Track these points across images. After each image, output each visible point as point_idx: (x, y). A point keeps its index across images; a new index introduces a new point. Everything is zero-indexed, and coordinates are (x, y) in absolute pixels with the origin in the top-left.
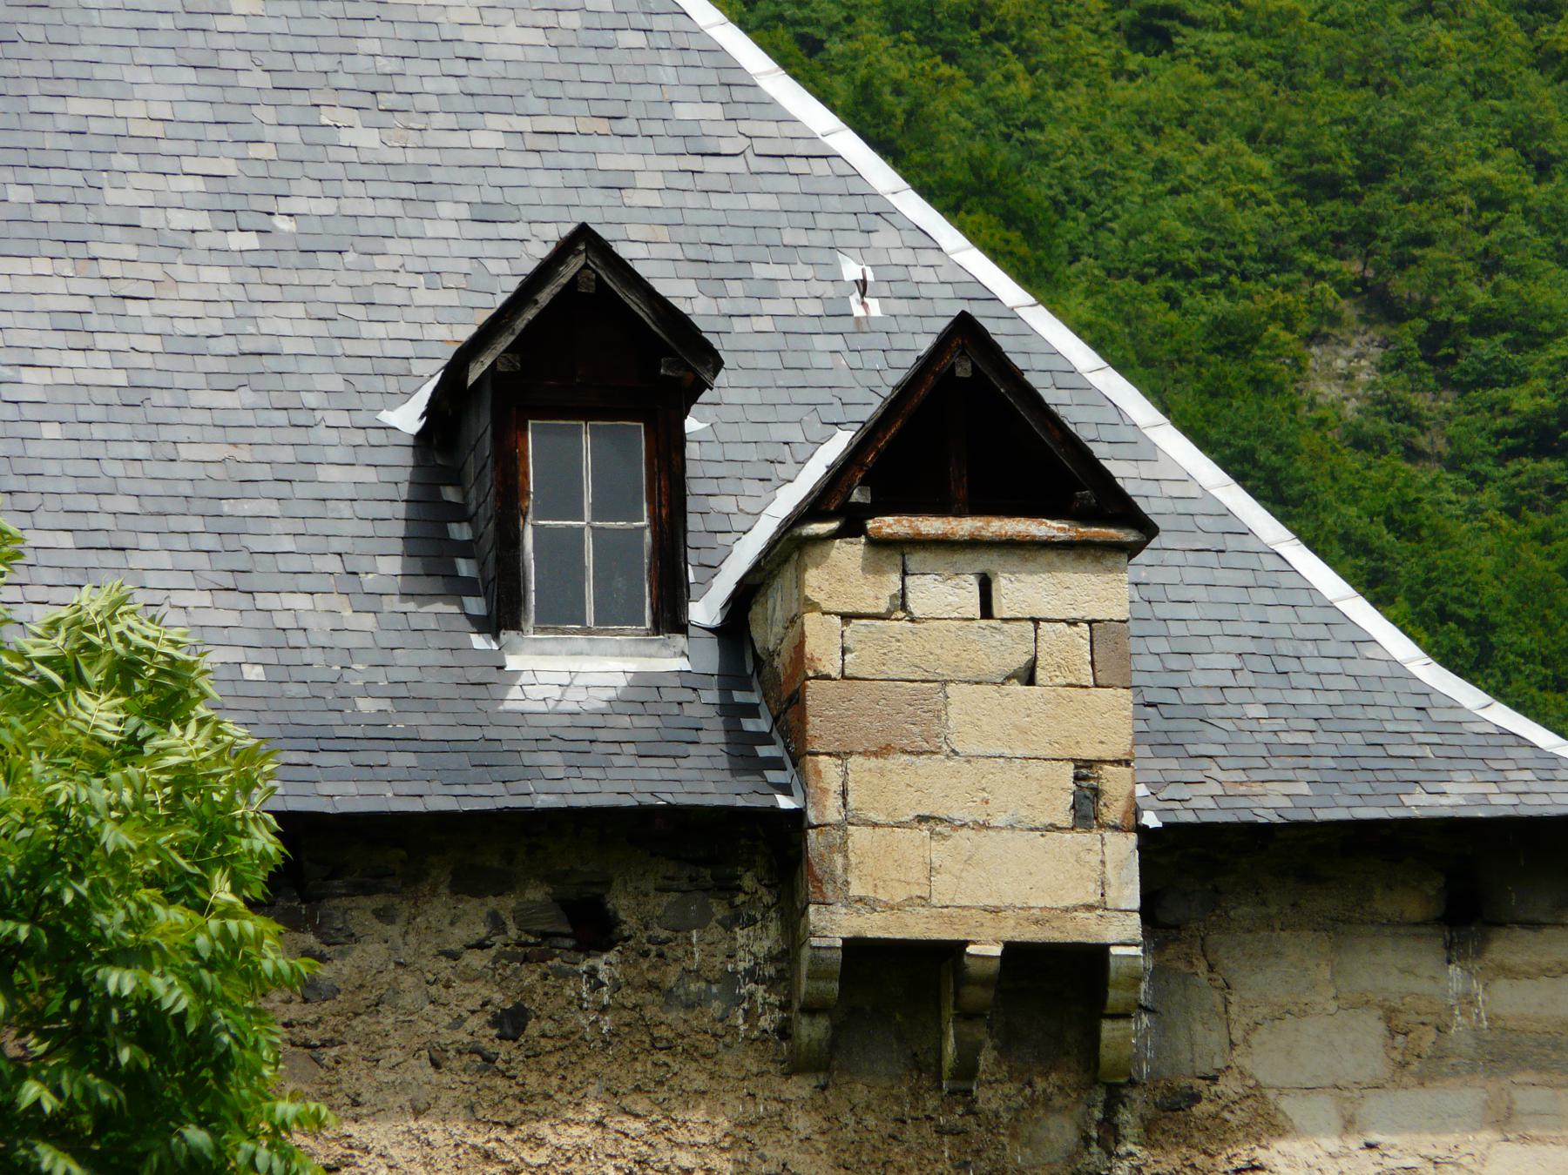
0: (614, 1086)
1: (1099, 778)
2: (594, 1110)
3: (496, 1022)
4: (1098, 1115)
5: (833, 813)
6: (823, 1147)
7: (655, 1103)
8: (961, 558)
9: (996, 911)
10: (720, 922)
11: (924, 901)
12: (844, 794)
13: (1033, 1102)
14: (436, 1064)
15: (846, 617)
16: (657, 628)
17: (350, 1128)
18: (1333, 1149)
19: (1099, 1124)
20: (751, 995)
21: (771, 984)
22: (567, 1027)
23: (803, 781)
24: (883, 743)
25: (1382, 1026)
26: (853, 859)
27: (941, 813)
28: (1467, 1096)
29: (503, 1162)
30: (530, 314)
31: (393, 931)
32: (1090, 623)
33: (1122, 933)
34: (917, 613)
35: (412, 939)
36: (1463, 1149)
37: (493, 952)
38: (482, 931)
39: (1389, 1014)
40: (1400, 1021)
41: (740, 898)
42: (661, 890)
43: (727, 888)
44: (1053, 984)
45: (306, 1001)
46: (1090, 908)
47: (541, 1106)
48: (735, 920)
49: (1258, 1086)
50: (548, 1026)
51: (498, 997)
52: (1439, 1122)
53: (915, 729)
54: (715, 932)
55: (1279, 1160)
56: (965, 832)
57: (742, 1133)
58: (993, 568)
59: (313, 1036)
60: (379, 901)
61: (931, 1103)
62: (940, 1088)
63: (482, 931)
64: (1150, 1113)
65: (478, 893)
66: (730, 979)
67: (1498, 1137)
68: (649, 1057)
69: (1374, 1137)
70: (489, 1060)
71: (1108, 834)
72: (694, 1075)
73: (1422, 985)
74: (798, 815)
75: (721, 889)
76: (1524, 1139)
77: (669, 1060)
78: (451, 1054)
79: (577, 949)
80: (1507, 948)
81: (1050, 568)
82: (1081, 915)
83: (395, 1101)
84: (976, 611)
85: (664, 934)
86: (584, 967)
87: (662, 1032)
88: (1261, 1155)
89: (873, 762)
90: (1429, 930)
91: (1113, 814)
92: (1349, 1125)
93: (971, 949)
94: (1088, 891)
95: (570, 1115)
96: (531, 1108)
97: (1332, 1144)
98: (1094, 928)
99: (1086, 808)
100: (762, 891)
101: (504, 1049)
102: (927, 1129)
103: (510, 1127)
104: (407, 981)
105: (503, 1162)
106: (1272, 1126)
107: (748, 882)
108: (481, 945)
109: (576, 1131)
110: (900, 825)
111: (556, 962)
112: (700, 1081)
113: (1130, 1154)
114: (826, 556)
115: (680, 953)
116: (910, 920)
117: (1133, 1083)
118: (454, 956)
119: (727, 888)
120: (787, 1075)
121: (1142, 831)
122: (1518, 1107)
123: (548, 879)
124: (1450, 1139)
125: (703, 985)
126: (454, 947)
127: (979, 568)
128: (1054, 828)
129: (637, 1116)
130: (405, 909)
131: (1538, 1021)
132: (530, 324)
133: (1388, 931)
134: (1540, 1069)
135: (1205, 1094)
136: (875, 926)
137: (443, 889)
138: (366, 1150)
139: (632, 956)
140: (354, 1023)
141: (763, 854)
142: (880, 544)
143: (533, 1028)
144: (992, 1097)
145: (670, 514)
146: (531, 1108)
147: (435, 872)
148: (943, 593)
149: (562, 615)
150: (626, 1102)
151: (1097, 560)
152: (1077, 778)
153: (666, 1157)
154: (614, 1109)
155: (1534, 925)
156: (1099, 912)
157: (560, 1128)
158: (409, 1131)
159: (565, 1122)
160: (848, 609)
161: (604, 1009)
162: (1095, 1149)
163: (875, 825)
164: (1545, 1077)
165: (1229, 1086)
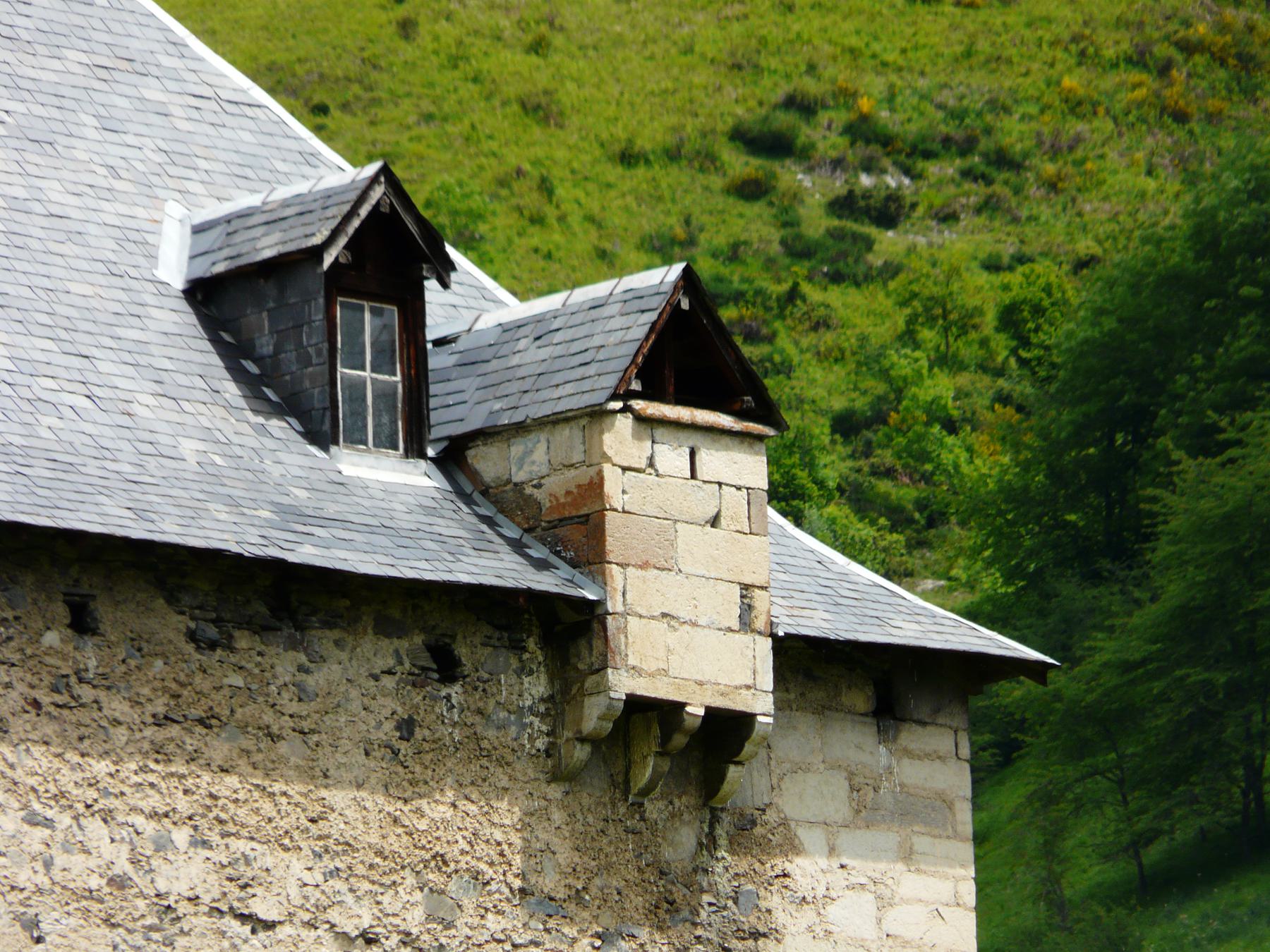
0: (461, 779)
1: (751, 598)
2: (450, 794)
3: (398, 728)
4: (706, 830)
5: (620, 608)
6: (567, 835)
7: (482, 794)
8: (683, 435)
9: (701, 684)
10: (515, 671)
11: (665, 672)
12: (624, 594)
13: (673, 816)
14: (367, 754)
15: (625, 469)
16: (407, 454)
17: (324, 793)
18: (824, 867)
19: (707, 835)
20: (531, 723)
21: (543, 717)
22: (437, 736)
23: (600, 579)
24: (644, 558)
25: (846, 784)
26: (630, 639)
27: (673, 613)
28: (888, 838)
29: (404, 826)
30: (356, 223)
31: (344, 656)
32: (748, 489)
33: (762, 705)
34: (661, 472)
35: (354, 662)
36: (889, 874)
37: (397, 677)
38: (391, 662)
39: (851, 776)
40: (858, 780)
41: (526, 656)
42: (484, 645)
43: (517, 647)
44: (727, 731)
45: (300, 700)
46: (748, 687)
47: (423, 789)
48: (523, 670)
49: (786, 818)
50: (427, 732)
51: (399, 710)
52: (875, 854)
53: (661, 552)
54: (514, 679)
55: (798, 871)
56: (686, 627)
57: (527, 820)
58: (698, 444)
59: (306, 725)
60: (336, 634)
61: (622, 810)
62: (626, 800)
63: (391, 662)
64: (732, 830)
65: (388, 636)
66: (520, 711)
67: (905, 868)
68: (480, 763)
69: (845, 861)
70: (396, 753)
71: (757, 637)
72: (501, 776)
73: (865, 757)
74: (600, 603)
75: (514, 648)
76: (918, 870)
77: (487, 764)
78: (376, 747)
79: (439, 681)
80: (911, 737)
81: (727, 448)
82: (744, 691)
83: (347, 776)
84: (688, 475)
85: (486, 676)
86: (443, 693)
87: (485, 744)
88: (789, 867)
89: (640, 572)
90: (868, 720)
91: (760, 624)
92: (832, 851)
93: (688, 709)
94: (738, 674)
95: (438, 797)
96: (417, 790)
97: (823, 862)
98: (750, 702)
99: (746, 623)
100: (539, 652)
101: (403, 747)
102: (620, 829)
103: (406, 801)
104: (354, 693)
105: (404, 826)
106: (792, 847)
107: (531, 644)
108: (390, 672)
109: (441, 808)
110: (653, 618)
111: (429, 688)
112: (505, 782)
113: (723, 858)
114: (613, 425)
115: (495, 690)
116: (659, 685)
117: (722, 810)
118: (376, 678)
119: (517, 647)
120: (549, 782)
121: (773, 636)
122: (916, 848)
123: (423, 630)
124: (882, 866)
125: (506, 714)
126: (377, 671)
127: (691, 444)
128: (730, 630)
129: (473, 802)
130: (350, 639)
131: (925, 790)
132: (357, 231)
133: (849, 717)
134: (926, 824)
135: (759, 821)
136: (645, 688)
137: (370, 631)
138: (333, 810)
139: (470, 689)
140: (325, 718)
141: (568, 632)
142: (640, 419)
143: (419, 734)
144: (654, 809)
145: (417, 374)
146: (417, 790)
147: (365, 618)
148: (672, 457)
149: (356, 439)
150: (467, 791)
151: (751, 445)
152: (742, 597)
153: (488, 831)
154: (461, 796)
155: (923, 724)
156: (753, 691)
157: (433, 805)
158: (355, 799)
159: (435, 801)
160: (626, 464)
161: (454, 725)
162: (705, 852)
163: (641, 616)
164: (928, 829)
165: (771, 816)
